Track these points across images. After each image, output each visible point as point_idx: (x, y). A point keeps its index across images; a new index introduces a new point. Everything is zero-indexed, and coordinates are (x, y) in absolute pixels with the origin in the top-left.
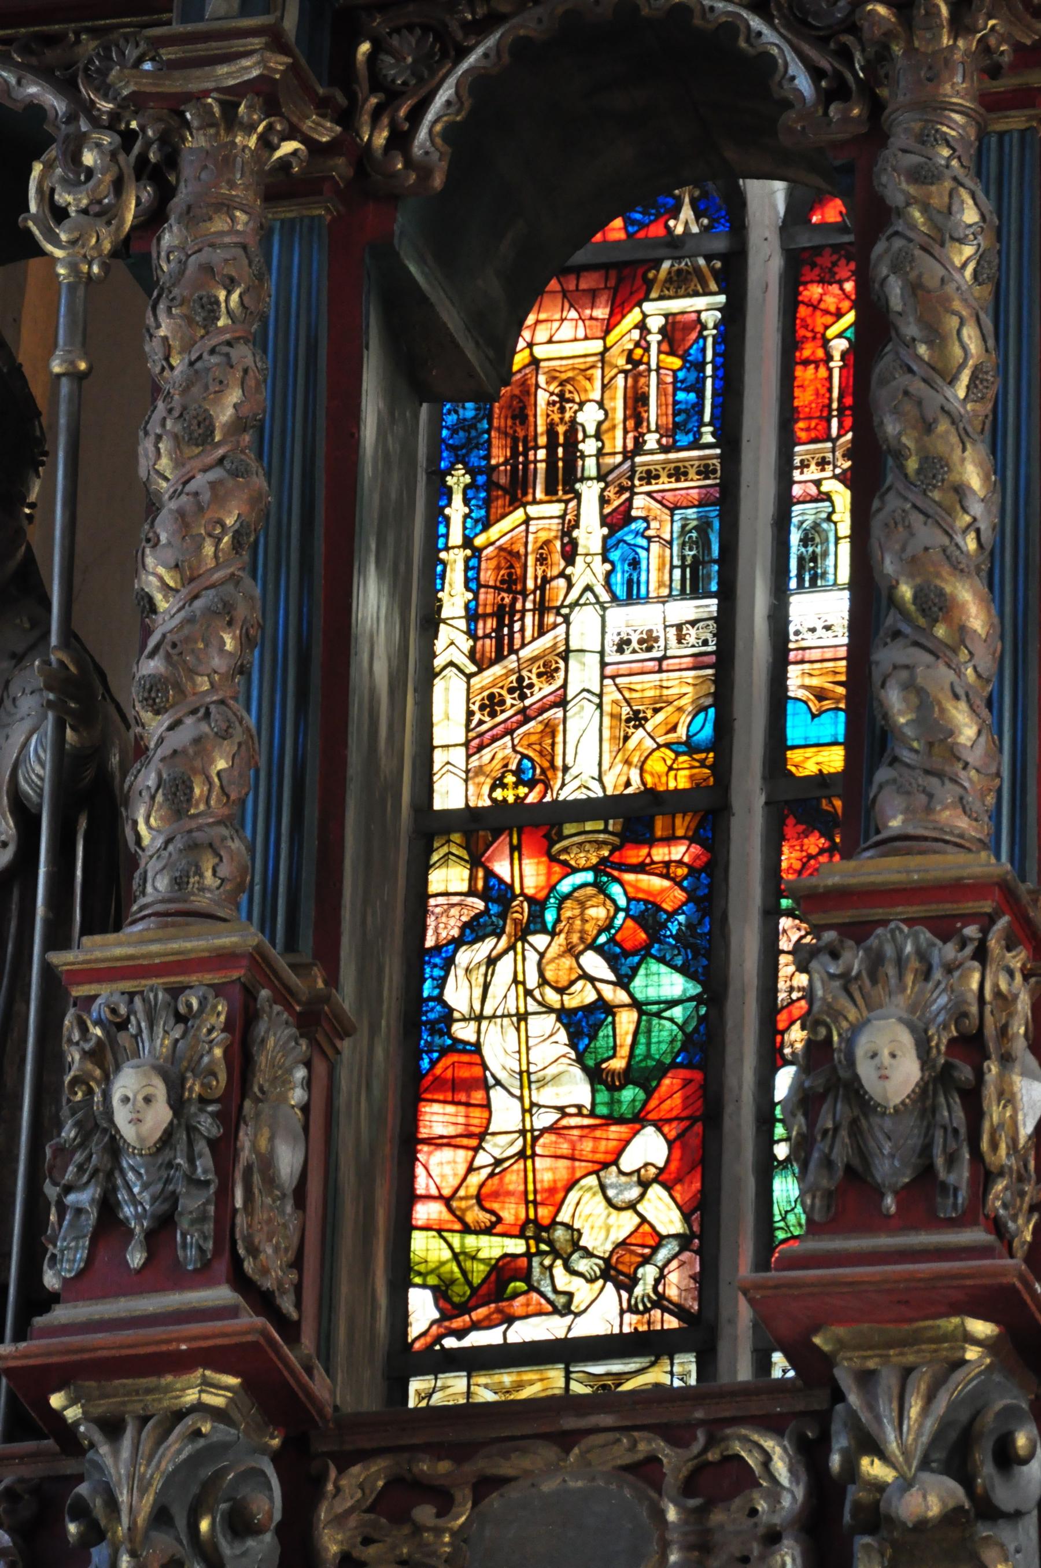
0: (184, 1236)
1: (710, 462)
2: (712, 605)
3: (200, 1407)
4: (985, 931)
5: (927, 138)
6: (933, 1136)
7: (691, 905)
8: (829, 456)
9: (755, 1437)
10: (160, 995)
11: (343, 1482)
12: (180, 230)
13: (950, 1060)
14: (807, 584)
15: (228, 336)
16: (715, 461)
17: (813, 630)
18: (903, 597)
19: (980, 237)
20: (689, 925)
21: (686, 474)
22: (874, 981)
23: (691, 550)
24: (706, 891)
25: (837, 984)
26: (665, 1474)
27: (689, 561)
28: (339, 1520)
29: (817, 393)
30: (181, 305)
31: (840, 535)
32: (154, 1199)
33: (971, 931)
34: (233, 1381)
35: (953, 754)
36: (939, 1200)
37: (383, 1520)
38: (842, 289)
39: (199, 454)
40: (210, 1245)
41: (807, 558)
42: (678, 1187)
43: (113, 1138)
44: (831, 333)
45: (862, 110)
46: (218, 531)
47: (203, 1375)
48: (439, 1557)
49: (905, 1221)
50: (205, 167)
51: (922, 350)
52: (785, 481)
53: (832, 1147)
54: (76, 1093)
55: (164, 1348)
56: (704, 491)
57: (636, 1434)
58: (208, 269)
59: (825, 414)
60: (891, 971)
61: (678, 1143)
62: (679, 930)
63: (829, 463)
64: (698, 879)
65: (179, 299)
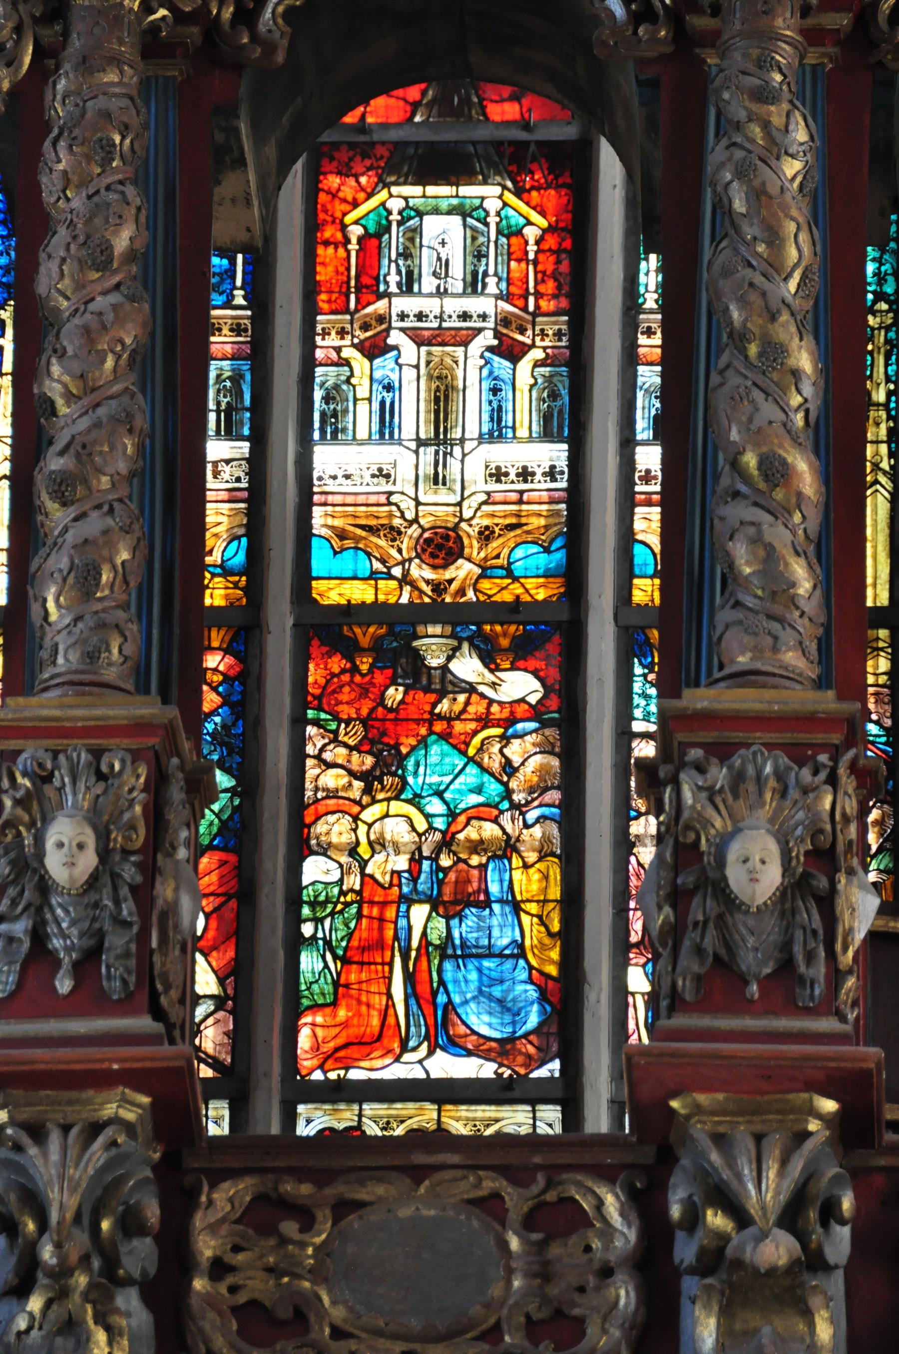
0: (108, 967)
1: (242, 321)
2: (244, 448)
3: (116, 1120)
4: (835, 759)
5: (764, 64)
6: (792, 935)
7: (226, 708)
8: (348, 327)
9: (590, 1183)
10: (83, 755)
11: (215, 1196)
12: (76, 78)
13: (809, 870)
14: (329, 437)
15: (120, 177)
16: (246, 321)
17: (335, 477)
18: (748, 463)
19: (808, 155)
20: (224, 726)
21: (220, 330)
22: (736, 796)
23: (225, 397)
24: (239, 697)
25: (704, 795)
26: (507, 1210)
27: (223, 407)
28: (213, 1228)
29: (337, 272)
30: (82, 144)
31: (358, 396)
32: (81, 935)
33: (823, 758)
34: (145, 1100)
35: (793, 600)
36: (798, 990)
37: (251, 1232)
38: (357, 182)
39: (99, 279)
40: (132, 979)
41: (329, 414)
42: (214, 954)
43: (42, 878)
44: (348, 219)
45: (667, 33)
46: (119, 348)
47: (123, 1093)
48: (304, 1268)
49: (765, 1008)
50: (98, 23)
51: (761, 248)
52: (309, 346)
53: (703, 937)
54: (6, 835)
55: (97, 1066)
56: (236, 346)
57: (481, 1173)
58: (106, 115)
59: (344, 290)
60: (751, 787)
61: (214, 915)
62: (215, 729)
63: (348, 333)
64: (232, 686)
65: (80, 139)
